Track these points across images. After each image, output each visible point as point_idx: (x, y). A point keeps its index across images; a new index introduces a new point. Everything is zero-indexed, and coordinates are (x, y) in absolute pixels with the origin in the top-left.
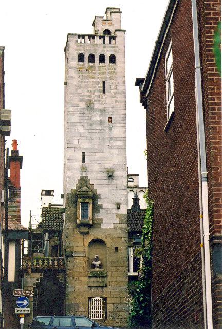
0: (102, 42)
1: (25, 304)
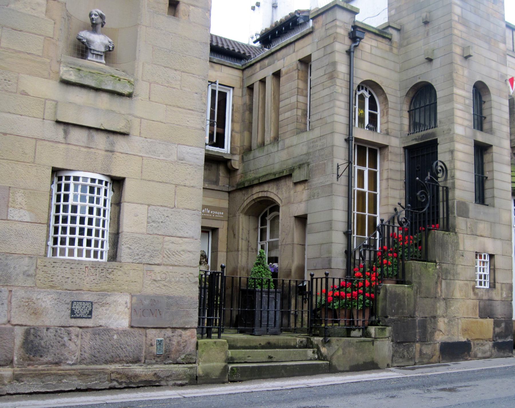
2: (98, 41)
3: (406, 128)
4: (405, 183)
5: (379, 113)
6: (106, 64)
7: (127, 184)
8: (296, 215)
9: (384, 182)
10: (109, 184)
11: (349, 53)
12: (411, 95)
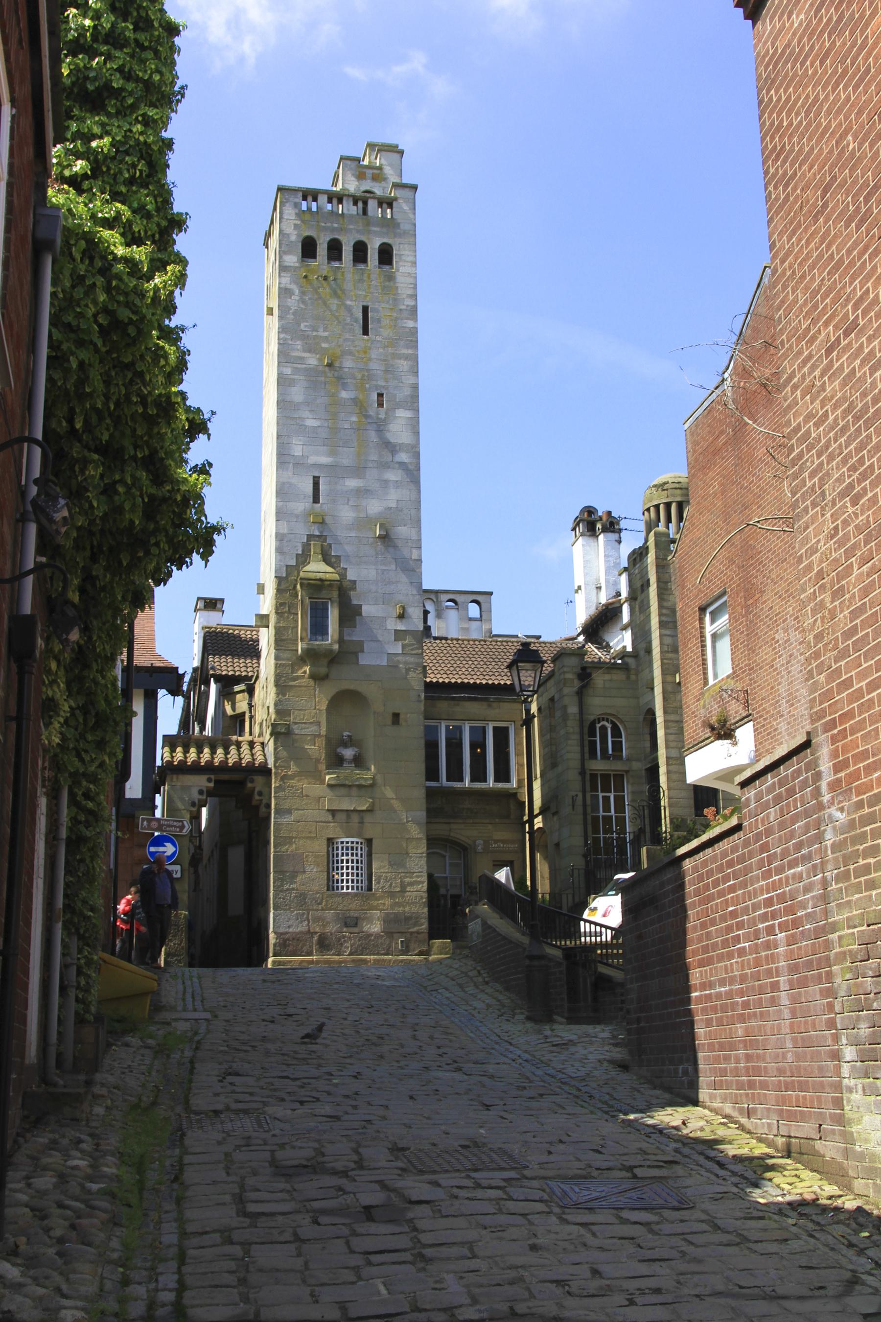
0: (361, 212)
1: (169, 853)
2: (348, 753)
7: (374, 842)
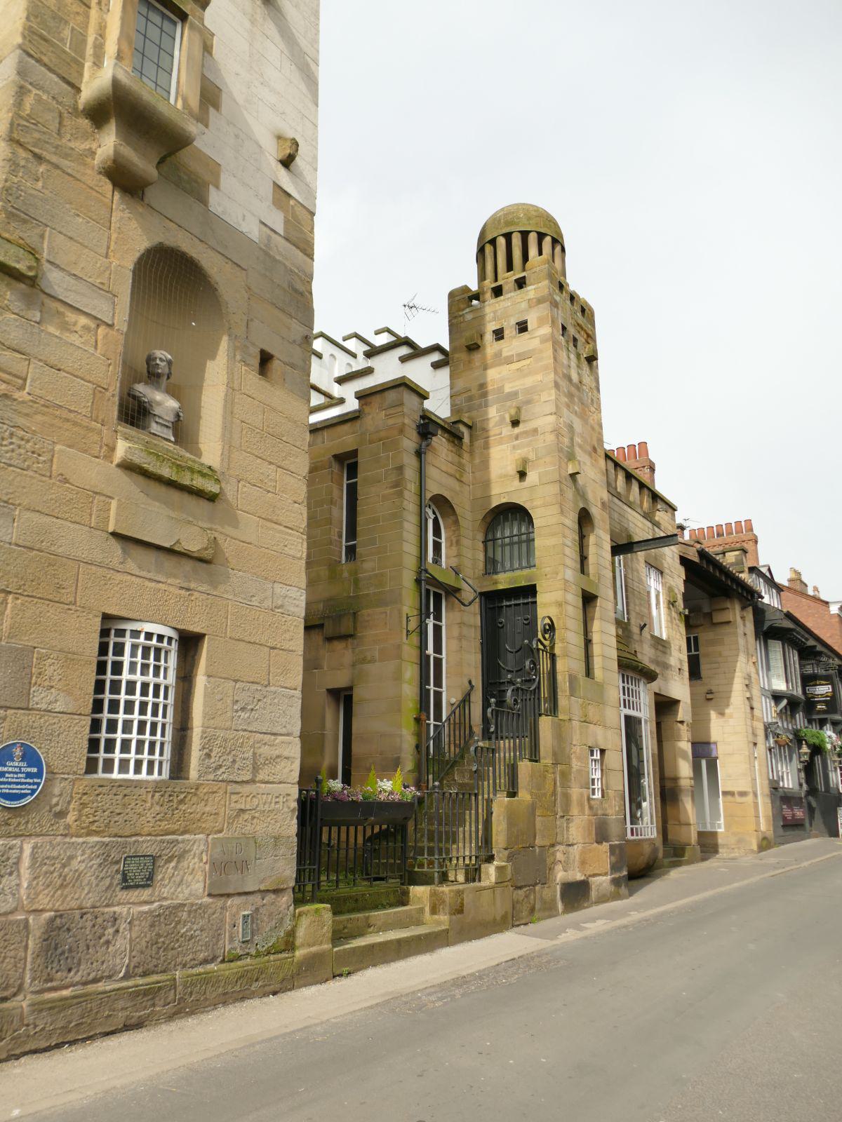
3: (481, 565)
4: (482, 644)
5: (443, 540)
6: (176, 443)
8: (330, 687)
9: (454, 643)
10: (173, 642)
11: (419, 454)
12: (489, 520)
